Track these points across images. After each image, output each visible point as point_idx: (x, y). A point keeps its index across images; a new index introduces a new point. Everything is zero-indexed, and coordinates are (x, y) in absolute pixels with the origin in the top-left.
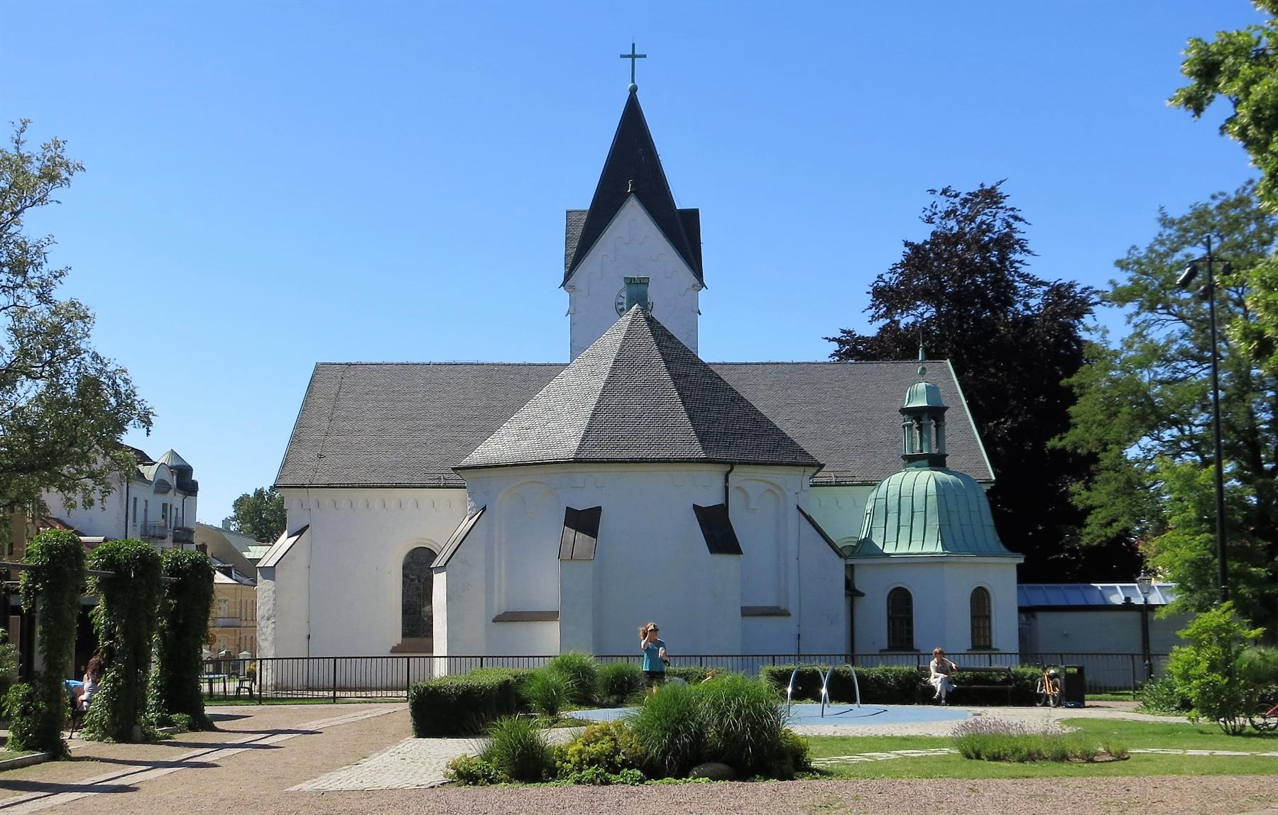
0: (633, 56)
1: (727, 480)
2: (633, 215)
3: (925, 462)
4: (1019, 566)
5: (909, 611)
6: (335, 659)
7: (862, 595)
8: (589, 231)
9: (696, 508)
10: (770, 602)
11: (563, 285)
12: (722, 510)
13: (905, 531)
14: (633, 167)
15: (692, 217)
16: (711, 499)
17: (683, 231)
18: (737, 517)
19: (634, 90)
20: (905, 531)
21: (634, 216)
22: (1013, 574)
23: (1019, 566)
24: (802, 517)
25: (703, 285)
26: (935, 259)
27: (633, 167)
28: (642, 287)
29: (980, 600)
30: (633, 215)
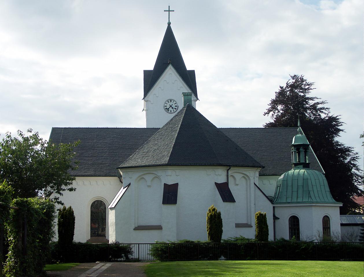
0: (169, 11)
1: (228, 173)
2: (170, 73)
3: (302, 166)
4: (340, 207)
5: (298, 225)
6: (139, 244)
7: (279, 219)
8: (151, 79)
9: (216, 183)
10: (244, 222)
11: (144, 99)
12: (226, 184)
13: (295, 194)
14: (170, 54)
15: (193, 73)
16: (222, 180)
17: (189, 78)
18: (231, 187)
19: (169, 24)
20: (295, 194)
21: (170, 74)
22: (338, 211)
23: (340, 207)
24: (256, 186)
25: (198, 99)
26: (16, 168)
27: (170, 54)
28: (189, 96)
29: (326, 221)
30: (170, 73)
